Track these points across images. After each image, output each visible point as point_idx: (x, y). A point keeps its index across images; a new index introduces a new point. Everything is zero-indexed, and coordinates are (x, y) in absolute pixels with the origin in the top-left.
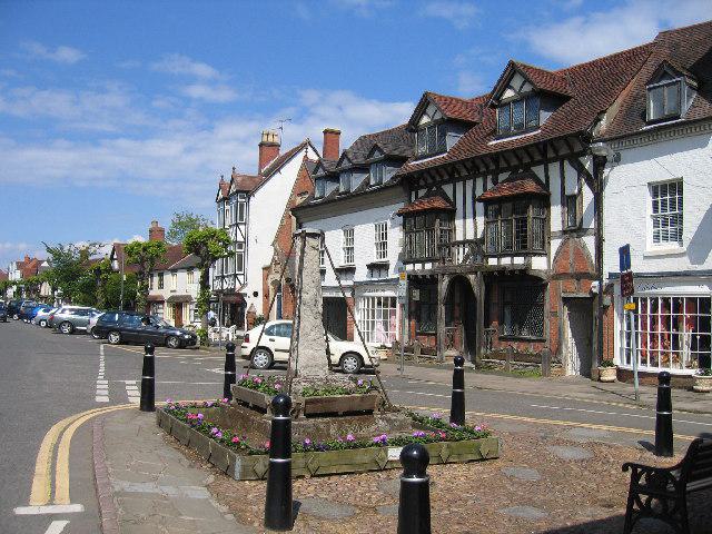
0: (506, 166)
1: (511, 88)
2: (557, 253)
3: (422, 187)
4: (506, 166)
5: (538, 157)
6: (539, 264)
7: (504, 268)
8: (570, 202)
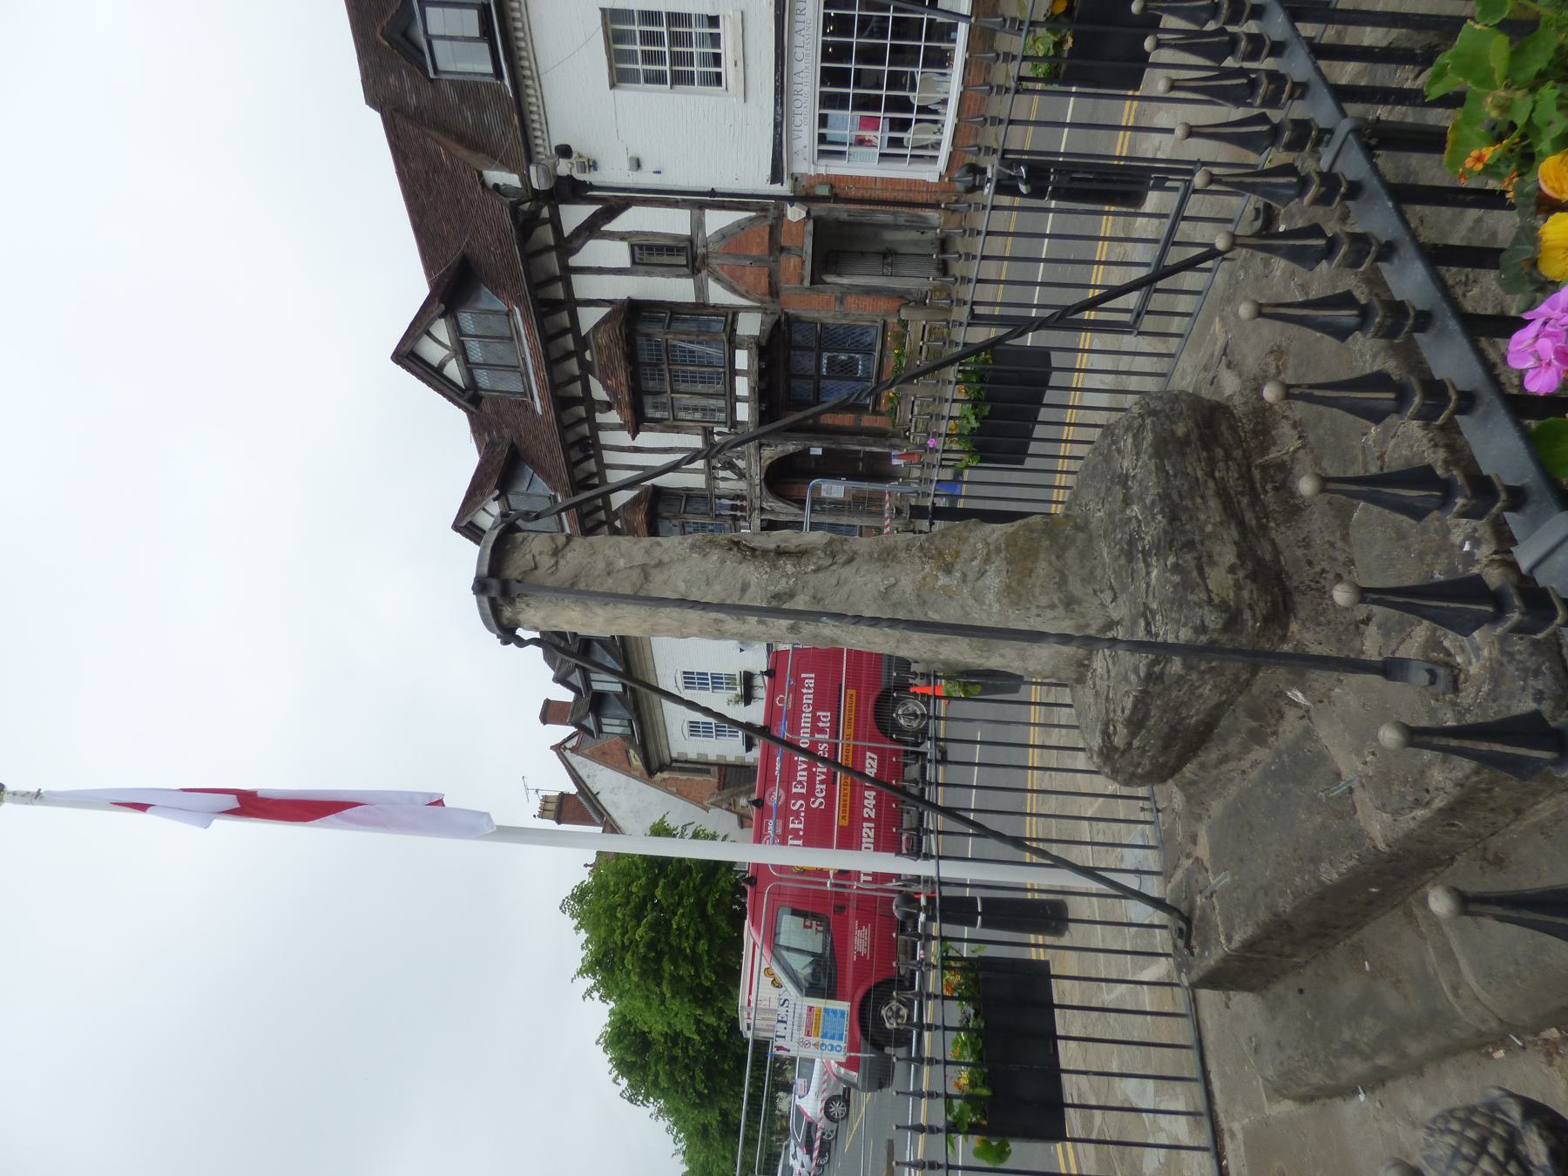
0: (579, 384)
1: (442, 365)
2: (734, 291)
3: (587, 388)
4: (579, 384)
5: (564, 319)
6: (750, 325)
7: (752, 389)
8: (650, 253)
